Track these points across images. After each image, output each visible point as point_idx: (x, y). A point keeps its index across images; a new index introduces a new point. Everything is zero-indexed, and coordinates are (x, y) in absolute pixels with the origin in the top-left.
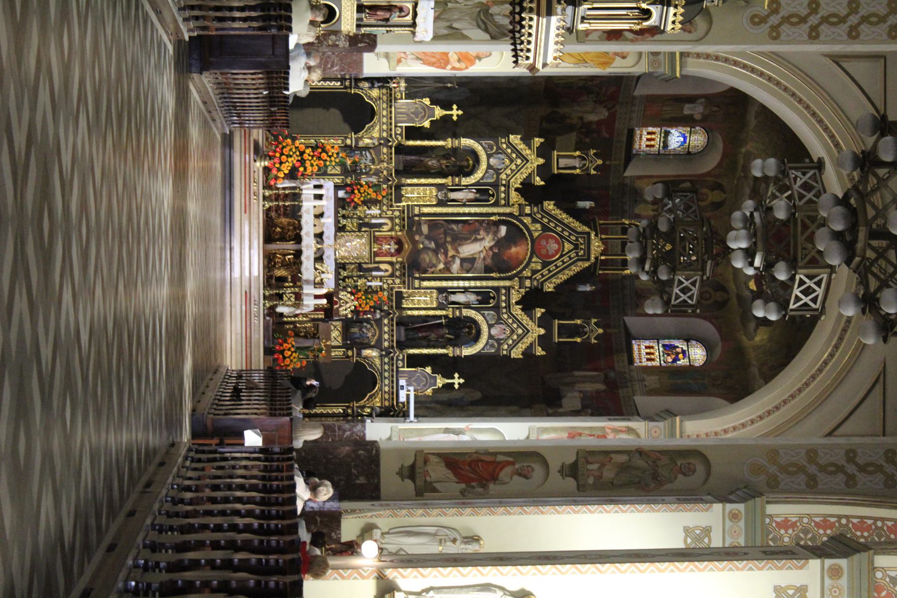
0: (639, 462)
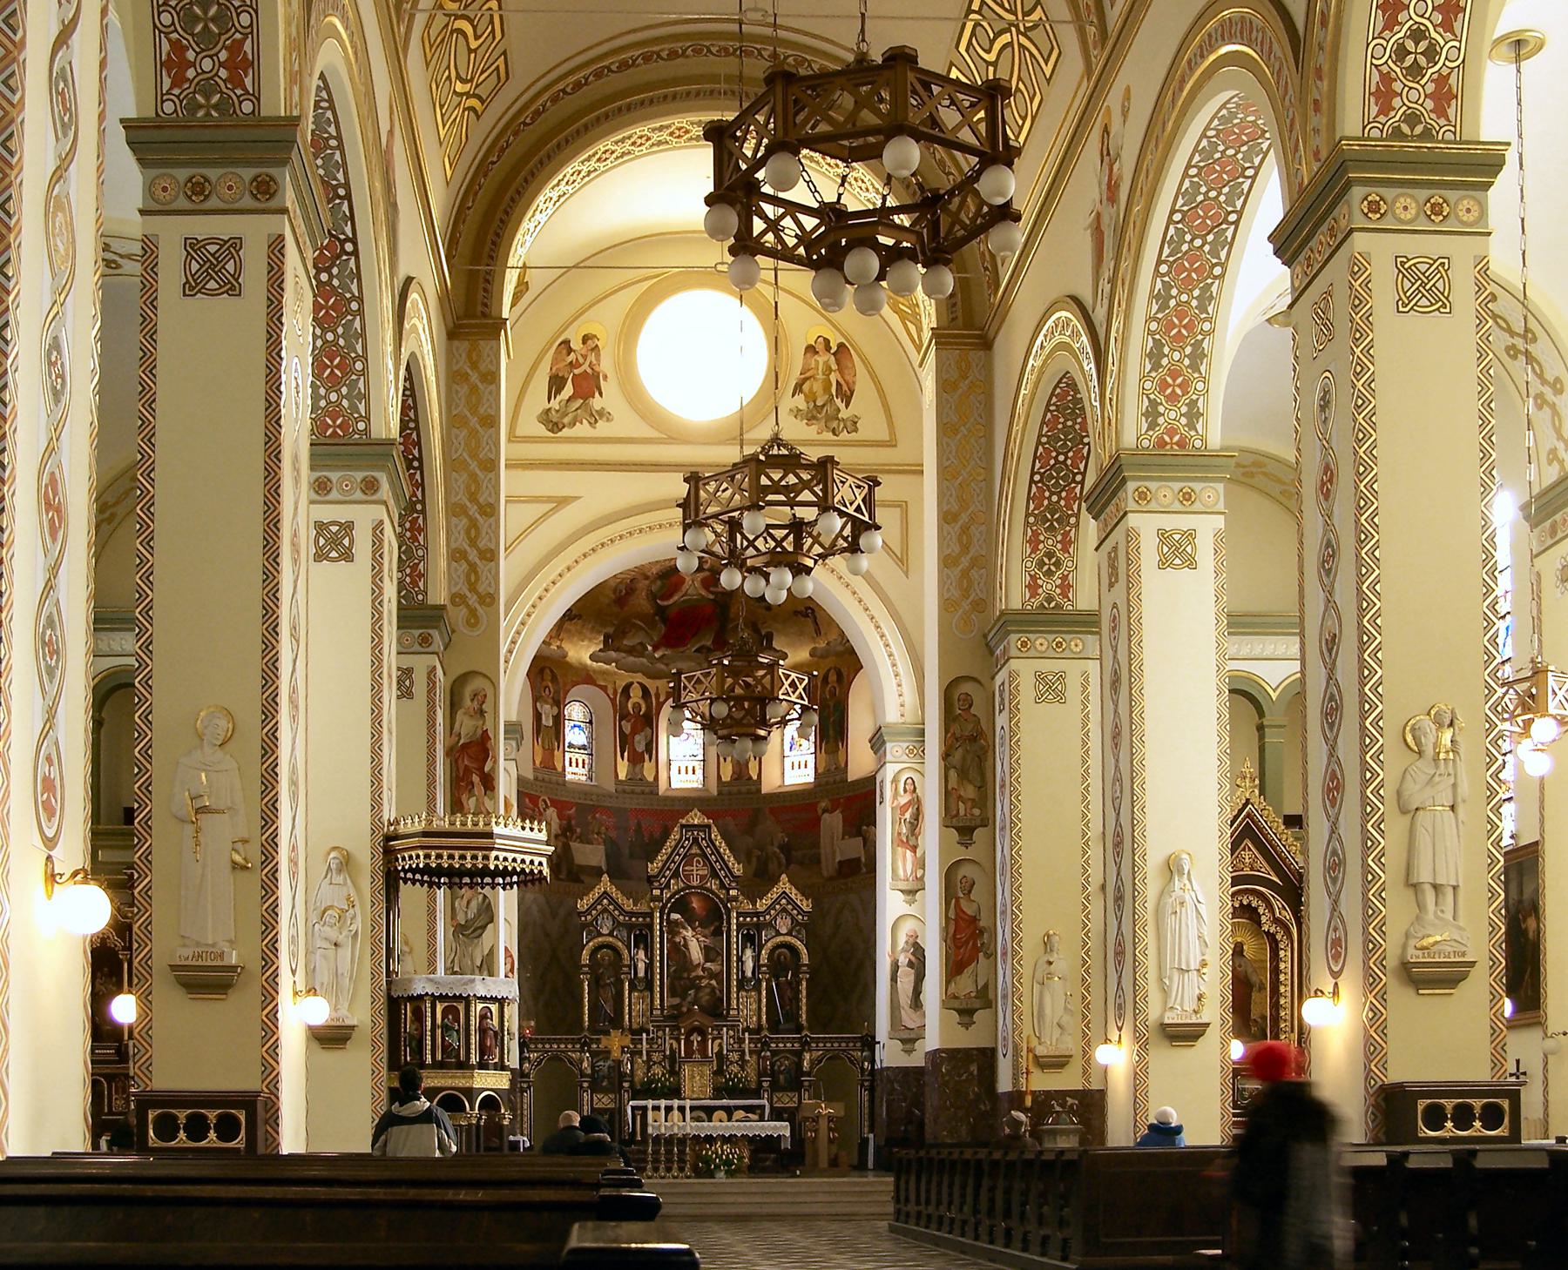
0: (957, 756)
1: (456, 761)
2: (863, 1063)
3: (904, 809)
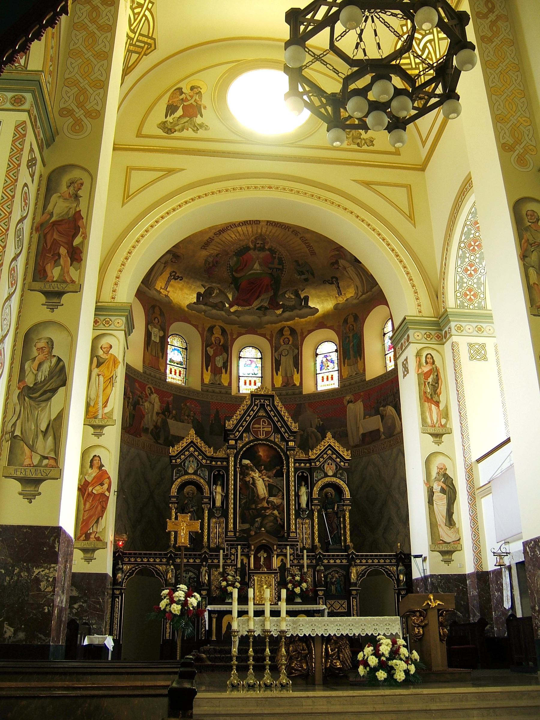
1: (45, 235)
2: (398, 576)
3: (427, 375)
